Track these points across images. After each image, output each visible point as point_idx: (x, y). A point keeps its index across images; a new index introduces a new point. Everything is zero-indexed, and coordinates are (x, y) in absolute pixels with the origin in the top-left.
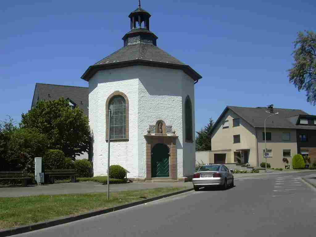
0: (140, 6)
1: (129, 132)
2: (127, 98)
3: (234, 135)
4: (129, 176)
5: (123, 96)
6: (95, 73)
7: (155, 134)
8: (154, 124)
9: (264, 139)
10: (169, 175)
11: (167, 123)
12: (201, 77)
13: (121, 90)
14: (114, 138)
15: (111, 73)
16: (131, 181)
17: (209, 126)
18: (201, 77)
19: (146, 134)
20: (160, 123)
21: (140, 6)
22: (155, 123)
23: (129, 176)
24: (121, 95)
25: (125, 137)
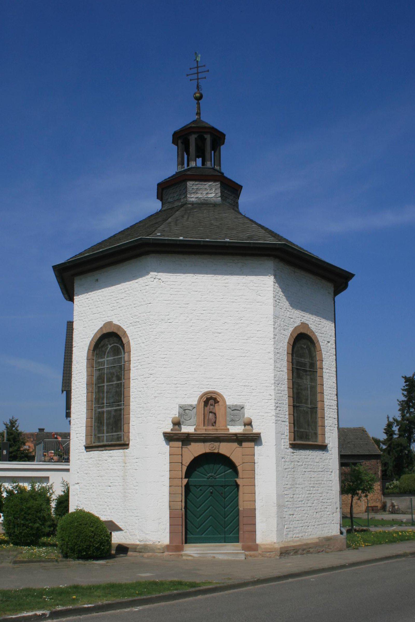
0: (198, 114)
1: (130, 425)
2: (126, 338)
3: (117, 453)
4: (117, 538)
5: (120, 334)
6: (147, 253)
7: (195, 430)
8: (194, 401)
9: (68, 470)
10: (238, 538)
11: (231, 400)
12: (353, 275)
13: (116, 322)
14: (103, 441)
15: (97, 280)
16: (123, 549)
17: (404, 396)
18: (353, 275)
19: (168, 428)
20: (210, 400)
21: (200, 114)
22: (197, 399)
23: (117, 538)
24: (115, 331)
25: (119, 438)
